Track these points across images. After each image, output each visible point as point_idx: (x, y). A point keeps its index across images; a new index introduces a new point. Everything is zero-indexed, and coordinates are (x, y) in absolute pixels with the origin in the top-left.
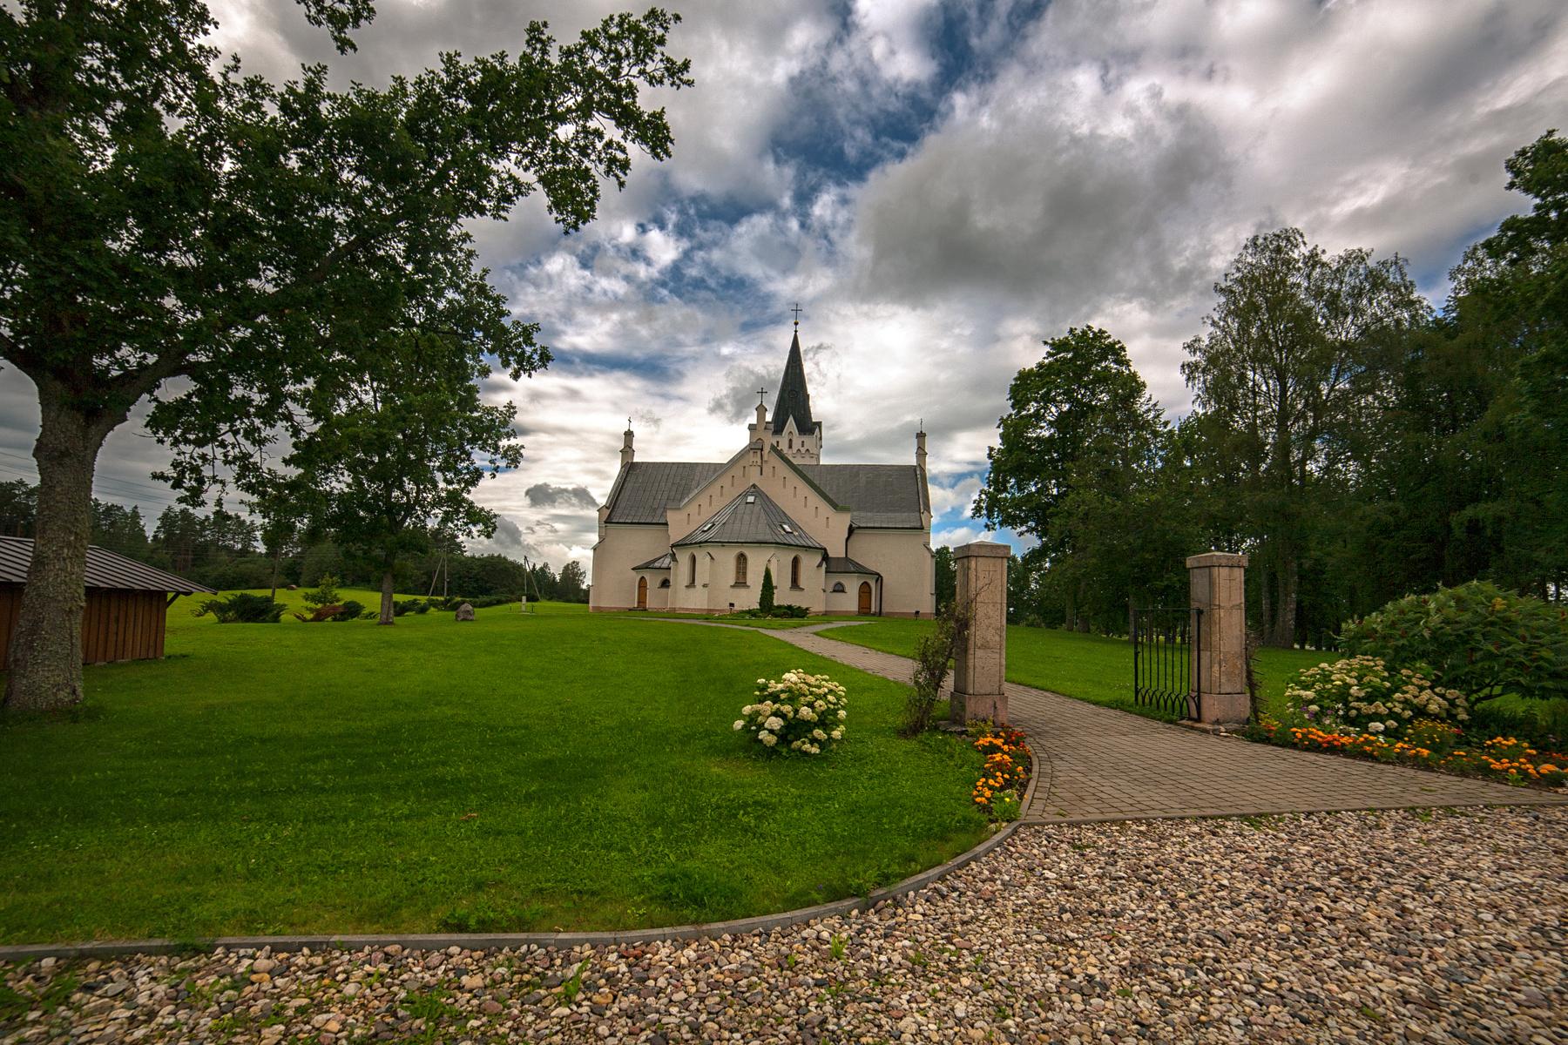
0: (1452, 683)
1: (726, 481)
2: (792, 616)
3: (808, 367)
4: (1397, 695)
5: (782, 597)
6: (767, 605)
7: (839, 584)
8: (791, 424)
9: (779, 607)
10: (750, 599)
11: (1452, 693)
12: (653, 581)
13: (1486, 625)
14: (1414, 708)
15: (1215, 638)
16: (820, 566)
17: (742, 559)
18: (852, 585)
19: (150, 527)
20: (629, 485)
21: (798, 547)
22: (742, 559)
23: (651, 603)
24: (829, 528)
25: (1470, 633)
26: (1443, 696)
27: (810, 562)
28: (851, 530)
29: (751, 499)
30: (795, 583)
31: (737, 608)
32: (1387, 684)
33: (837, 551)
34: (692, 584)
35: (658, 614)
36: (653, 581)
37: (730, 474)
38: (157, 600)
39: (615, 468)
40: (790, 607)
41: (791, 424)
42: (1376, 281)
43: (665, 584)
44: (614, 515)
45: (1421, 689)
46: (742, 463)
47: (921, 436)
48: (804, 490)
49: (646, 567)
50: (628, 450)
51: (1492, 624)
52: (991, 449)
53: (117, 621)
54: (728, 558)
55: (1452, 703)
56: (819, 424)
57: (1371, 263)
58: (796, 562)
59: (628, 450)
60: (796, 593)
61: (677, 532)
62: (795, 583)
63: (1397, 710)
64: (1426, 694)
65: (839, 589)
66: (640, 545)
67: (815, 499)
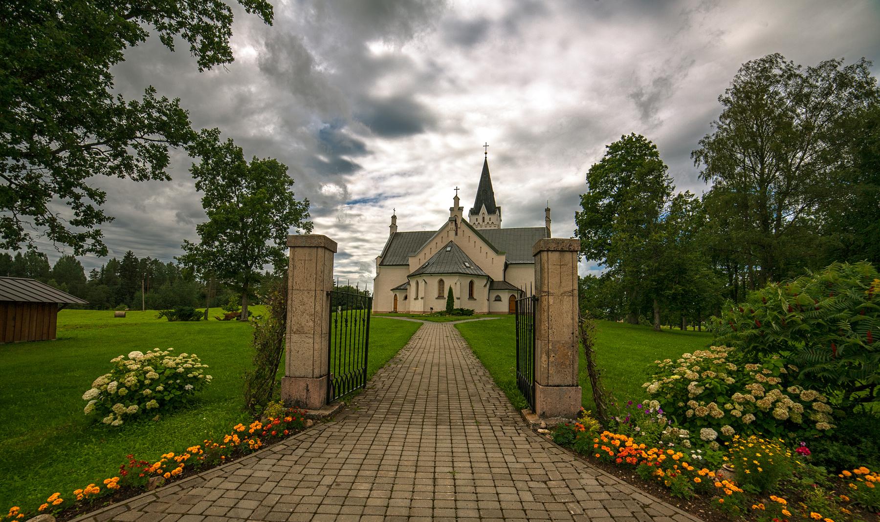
0: (811, 381)
1: (438, 240)
2: (463, 314)
3: (492, 175)
4: (737, 395)
5: (457, 305)
6: (450, 310)
7: (498, 296)
8: (484, 209)
9: (457, 309)
10: (441, 306)
11: (809, 394)
12: (400, 297)
13: (856, 312)
14: (757, 412)
15: (544, 326)
16: (485, 286)
17: (441, 282)
18: (505, 297)
19: (52, 264)
20: (393, 245)
21: (473, 276)
22: (441, 282)
23: (400, 309)
24: (493, 265)
25: (834, 321)
26: (796, 398)
27: (479, 284)
28: (506, 266)
29: (449, 249)
30: (471, 296)
31: (435, 310)
32: (731, 380)
33: (498, 276)
34: (416, 299)
35: (403, 315)
36: (400, 297)
37: (440, 236)
38: (53, 308)
39: (387, 235)
40: (462, 310)
41: (484, 209)
42: (843, 81)
43: (406, 298)
44: (383, 262)
45: (769, 388)
46: (447, 229)
47: (548, 210)
48: (480, 243)
49: (397, 289)
50: (393, 226)
51: (868, 311)
52: (577, 213)
53: (14, 319)
54: (434, 282)
55: (808, 406)
56: (499, 208)
57: (840, 69)
58: (471, 283)
59: (393, 226)
60: (472, 302)
61: (413, 268)
62: (471, 296)
63: (737, 413)
64: (771, 397)
65: (498, 299)
66: (397, 277)
67: (486, 248)
